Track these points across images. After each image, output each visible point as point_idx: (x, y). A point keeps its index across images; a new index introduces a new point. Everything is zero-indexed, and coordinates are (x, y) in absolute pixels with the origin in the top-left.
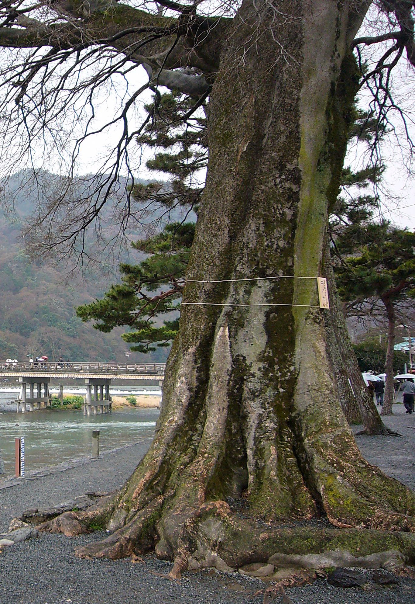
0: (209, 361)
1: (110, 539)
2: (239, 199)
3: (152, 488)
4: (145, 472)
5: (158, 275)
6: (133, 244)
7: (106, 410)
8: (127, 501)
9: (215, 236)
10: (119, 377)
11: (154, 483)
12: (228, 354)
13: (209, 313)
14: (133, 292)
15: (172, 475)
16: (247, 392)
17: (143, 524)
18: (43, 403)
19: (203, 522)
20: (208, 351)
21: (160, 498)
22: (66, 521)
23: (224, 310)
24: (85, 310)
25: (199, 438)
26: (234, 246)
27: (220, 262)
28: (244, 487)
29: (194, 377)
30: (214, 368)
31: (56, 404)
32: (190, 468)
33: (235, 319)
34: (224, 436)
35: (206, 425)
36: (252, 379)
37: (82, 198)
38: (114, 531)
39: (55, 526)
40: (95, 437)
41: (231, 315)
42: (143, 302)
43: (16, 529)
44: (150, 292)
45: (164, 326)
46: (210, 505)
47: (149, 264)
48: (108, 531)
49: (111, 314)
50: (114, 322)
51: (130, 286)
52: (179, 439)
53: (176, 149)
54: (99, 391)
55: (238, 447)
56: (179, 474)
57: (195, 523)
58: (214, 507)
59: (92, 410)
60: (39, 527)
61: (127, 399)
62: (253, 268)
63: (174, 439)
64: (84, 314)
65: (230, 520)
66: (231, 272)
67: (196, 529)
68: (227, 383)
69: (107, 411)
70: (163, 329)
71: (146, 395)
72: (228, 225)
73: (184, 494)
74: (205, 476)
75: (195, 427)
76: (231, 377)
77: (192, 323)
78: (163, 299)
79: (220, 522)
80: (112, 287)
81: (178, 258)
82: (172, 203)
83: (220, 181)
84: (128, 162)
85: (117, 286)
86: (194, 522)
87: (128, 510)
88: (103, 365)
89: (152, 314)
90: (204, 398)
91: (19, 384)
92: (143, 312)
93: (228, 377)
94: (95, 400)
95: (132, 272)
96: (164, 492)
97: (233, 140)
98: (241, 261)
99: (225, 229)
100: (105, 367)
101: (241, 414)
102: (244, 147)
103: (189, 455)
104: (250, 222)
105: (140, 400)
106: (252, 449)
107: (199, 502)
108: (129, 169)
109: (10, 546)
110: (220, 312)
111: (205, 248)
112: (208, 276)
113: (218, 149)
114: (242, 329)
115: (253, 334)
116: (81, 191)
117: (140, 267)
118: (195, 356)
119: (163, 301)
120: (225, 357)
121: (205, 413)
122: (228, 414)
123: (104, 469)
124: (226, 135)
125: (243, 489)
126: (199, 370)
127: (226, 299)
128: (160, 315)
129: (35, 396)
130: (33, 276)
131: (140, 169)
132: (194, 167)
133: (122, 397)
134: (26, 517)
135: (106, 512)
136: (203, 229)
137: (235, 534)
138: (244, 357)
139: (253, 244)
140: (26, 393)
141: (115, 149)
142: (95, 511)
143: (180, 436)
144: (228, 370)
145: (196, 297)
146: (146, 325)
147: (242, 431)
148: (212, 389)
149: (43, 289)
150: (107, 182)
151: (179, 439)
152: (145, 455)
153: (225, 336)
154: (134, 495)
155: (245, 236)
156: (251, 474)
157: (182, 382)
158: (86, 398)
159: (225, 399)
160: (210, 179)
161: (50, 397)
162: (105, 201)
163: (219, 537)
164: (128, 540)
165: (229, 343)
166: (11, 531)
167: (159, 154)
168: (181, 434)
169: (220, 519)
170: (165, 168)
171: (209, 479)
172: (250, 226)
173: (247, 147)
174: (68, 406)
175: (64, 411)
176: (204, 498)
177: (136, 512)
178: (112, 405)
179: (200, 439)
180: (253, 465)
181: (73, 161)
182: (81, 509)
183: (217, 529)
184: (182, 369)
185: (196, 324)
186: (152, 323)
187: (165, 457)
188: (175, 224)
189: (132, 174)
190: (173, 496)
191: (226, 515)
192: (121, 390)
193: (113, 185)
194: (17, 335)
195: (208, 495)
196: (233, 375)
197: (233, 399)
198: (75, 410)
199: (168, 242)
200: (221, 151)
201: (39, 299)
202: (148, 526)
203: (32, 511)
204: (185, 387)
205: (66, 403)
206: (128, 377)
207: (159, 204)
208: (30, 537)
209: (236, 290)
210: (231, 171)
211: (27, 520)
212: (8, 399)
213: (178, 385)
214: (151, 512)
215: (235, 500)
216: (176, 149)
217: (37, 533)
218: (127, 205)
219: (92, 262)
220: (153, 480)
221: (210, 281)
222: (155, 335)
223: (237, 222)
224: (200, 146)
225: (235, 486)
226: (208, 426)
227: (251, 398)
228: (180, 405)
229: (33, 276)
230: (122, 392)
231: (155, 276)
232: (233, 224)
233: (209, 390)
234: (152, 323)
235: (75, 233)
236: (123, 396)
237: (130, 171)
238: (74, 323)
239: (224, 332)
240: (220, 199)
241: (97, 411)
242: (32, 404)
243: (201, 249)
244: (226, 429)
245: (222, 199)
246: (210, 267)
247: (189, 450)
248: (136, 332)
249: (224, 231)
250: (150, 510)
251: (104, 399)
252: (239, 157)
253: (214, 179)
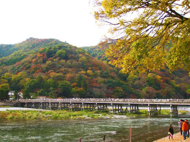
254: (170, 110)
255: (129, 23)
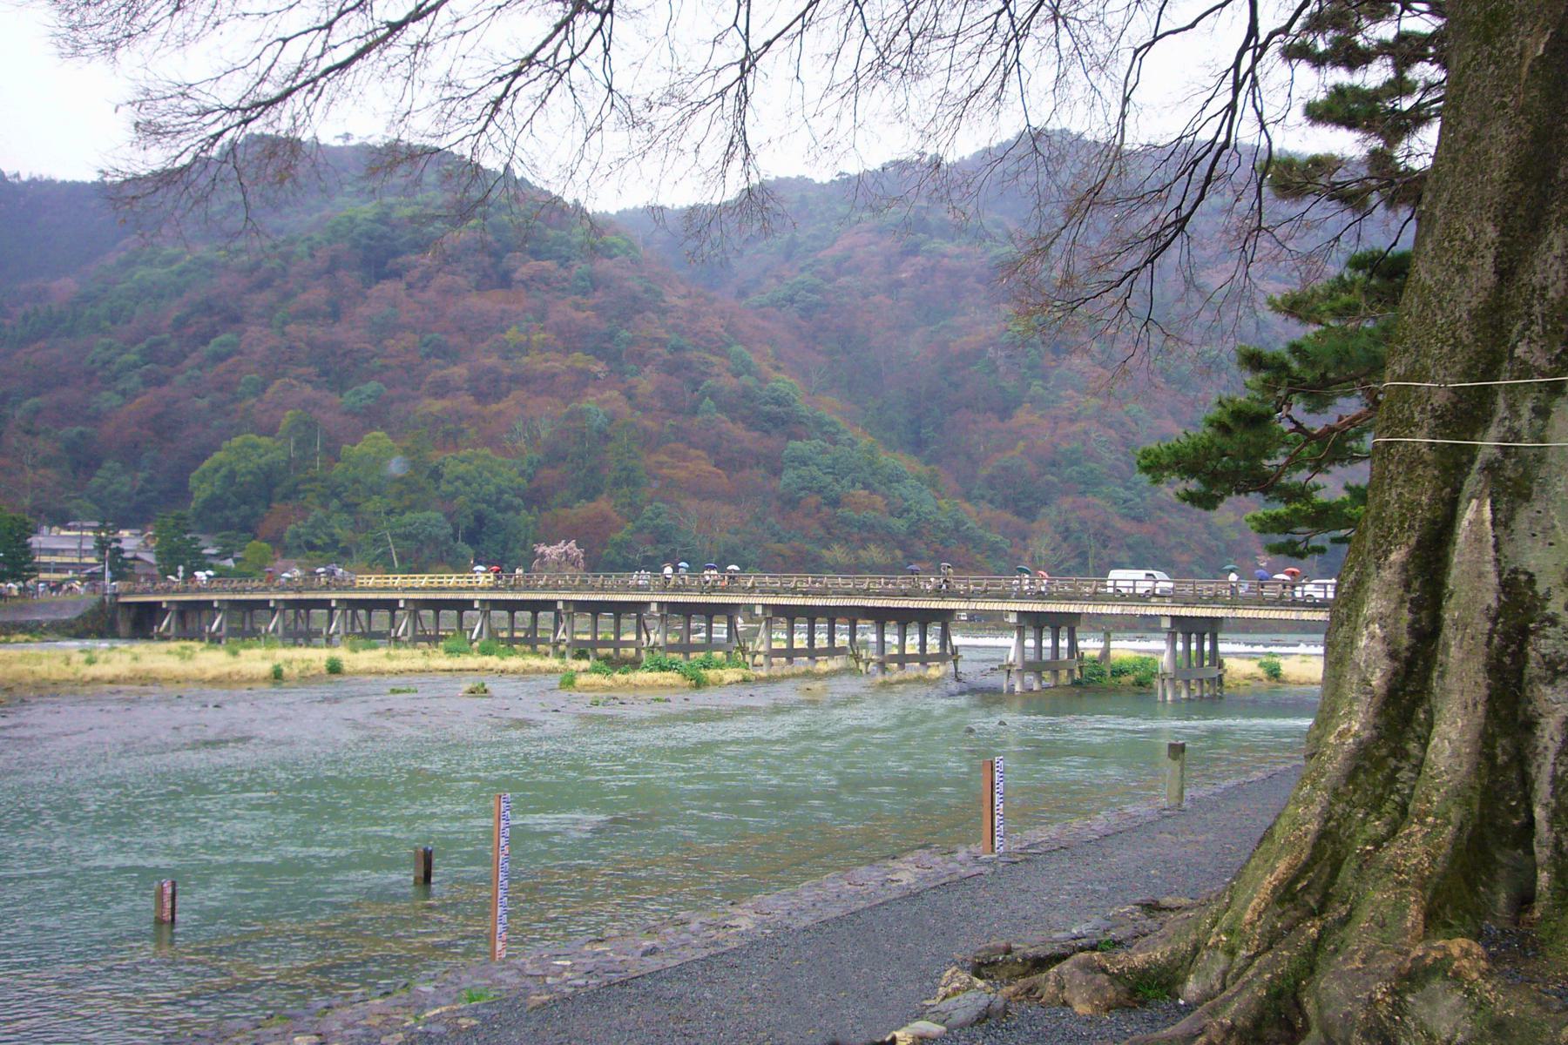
0: (1442, 585)
1: (1183, 1025)
2: (1522, 177)
3: (1293, 898)
4: (1278, 858)
5: (1332, 375)
6: (1271, 302)
7: (1208, 691)
8: (1230, 932)
9: (1461, 270)
10: (1241, 613)
11: (1299, 886)
12: (1489, 568)
13: (1442, 464)
14: (1269, 416)
15: (1344, 867)
16: (1538, 663)
17: (1268, 989)
18: (1064, 673)
19: (1418, 993)
20: (1438, 560)
21: (1313, 926)
22: (1079, 977)
23: (1480, 456)
24: (1157, 456)
25: (1413, 775)
26: (1508, 296)
27: (1471, 336)
28: (1525, 899)
29: (1404, 625)
30: (1453, 601)
31: (1094, 675)
32: (1390, 852)
33: (1509, 479)
34: (1476, 770)
35: (1433, 743)
36: (1550, 631)
37: (1147, 188)
38: (1199, 1003)
39: (1050, 988)
40: (1175, 759)
41: (1499, 468)
42: (1296, 438)
43: (955, 994)
44: (1313, 415)
45: (1346, 495)
46: (1434, 948)
47: (1309, 348)
48: (1181, 1002)
49: (1219, 466)
50: (1227, 486)
51: (1263, 402)
52: (1362, 776)
53: (1376, 75)
54: (1194, 646)
55: (1512, 800)
56: (1360, 866)
57: (1397, 993)
58: (1446, 956)
59: (1176, 691)
60: (1012, 989)
61: (1261, 665)
62: (1558, 351)
63: (1351, 776)
64: (1154, 467)
65: (1487, 989)
66: (1502, 361)
67: (1398, 1008)
68: (1485, 638)
69: (1211, 692)
70: (1343, 504)
71: (1304, 655)
72: (1493, 243)
73: (1372, 918)
74: (1427, 873)
75: (1403, 749)
76: (1496, 624)
77: (1399, 490)
78: (1344, 433)
79: (1461, 993)
80: (1220, 402)
81: (1377, 332)
82: (1364, 202)
83: (1476, 131)
84: (1258, 101)
85: (1232, 401)
86: (1393, 992)
87: (1232, 952)
88: (1205, 586)
89: (1317, 468)
90: (1426, 678)
91: (1011, 628)
92: (1295, 463)
93: (1488, 625)
94: (1184, 666)
95: (1266, 368)
96: (1322, 908)
97: (1509, 26)
98: (1527, 333)
99: (1486, 252)
100: (1210, 589)
101: (1521, 718)
102: (1537, 45)
103: (1387, 818)
104: (1551, 236)
105: (1289, 668)
106: (1546, 805)
107: (1408, 939)
108: (1261, 120)
109: (935, 1040)
110: (1472, 461)
111: (1434, 301)
112: (1442, 373)
113: (1471, 52)
114: (1525, 504)
115: (1552, 518)
116: (1143, 175)
117: (1287, 356)
118: (1407, 571)
119: (1344, 437)
120: (1481, 575)
121: (1430, 713)
122: (1487, 717)
123: (1191, 837)
124: (1494, 17)
125: (1523, 904)
126: (1416, 606)
127: (1486, 429)
128: (1336, 469)
129: (1047, 656)
130: (1045, 378)
131: (1290, 120)
132: (1418, 118)
133: (1250, 659)
134: (981, 964)
135: (1179, 956)
136: (1431, 254)
137: (1499, 1027)
138: (1531, 576)
139: (1557, 292)
140: (1024, 647)
141: (1228, 71)
142: (1155, 952)
143: (1366, 771)
144: (1489, 608)
145: (1409, 424)
146: (1303, 493)
147: (1522, 760)
148: (1447, 655)
149: (1069, 408)
150: (1209, 150)
151: (1362, 776)
152: (1278, 816)
153: (1483, 522)
154: (1248, 916)
155: (1538, 269)
156: (1543, 869)
157: (1372, 637)
158: (1165, 660)
159: (1479, 680)
160: (1451, 126)
161: (1081, 658)
162: (1202, 197)
163: (1457, 1030)
164: (1230, 1031)
165: (1492, 540)
166: (943, 1000)
167: (1335, 87)
168: (1367, 764)
169: (1461, 986)
170: (1350, 119)
171: (1435, 880)
172: (1551, 244)
173: (1546, 44)
174: (1123, 679)
175: (1115, 691)
176: (1421, 927)
177: (1253, 958)
178: (1226, 678)
179: (1416, 779)
180: (1547, 846)
181: (1126, 100)
182: (1120, 943)
183: (1454, 1011)
184: (1373, 604)
185: (1410, 492)
186: (1317, 488)
187: (1327, 821)
188: (1372, 253)
189: (1270, 133)
190: (1345, 921)
191: (1475, 975)
192: (1247, 644)
193: (1223, 158)
194: (1008, 516)
195: (1434, 920)
196: (1501, 620)
197: (1501, 679)
198: (1137, 689)
199: (1356, 297)
200: (1479, 56)
201: (1058, 431)
202: (1279, 995)
203: (995, 950)
204: (1379, 647)
205: (1119, 672)
206: (1262, 614)
207: (1333, 204)
208: (987, 1017)
209: (1513, 409)
210: (1504, 106)
211: (983, 971)
212: (983, 661)
213: (1362, 643)
214: (1289, 958)
215: (1503, 932)
216: (1376, 75)
217: (1005, 1006)
218: (1256, 206)
219: (1171, 343)
220: (1296, 880)
221: (1446, 383)
222: (1325, 517)
223: (1518, 234)
224: (1436, 66)
225: (1502, 898)
226: (1435, 746)
227: (1545, 678)
228: (1366, 693)
229: (1045, 378)
230: (1248, 649)
231: (1323, 376)
232: (1508, 239)
233: (1439, 657)
234: (1317, 488)
235: (1131, 272)
236: (1250, 656)
237: (1263, 127)
238: (1139, 487)
239: (1479, 511)
240: (1475, 177)
241: (1190, 691)
242: (1039, 674)
243: (1426, 304)
244: (1481, 753)
245: (1480, 177)
246: (1446, 349)
247: (1388, 807)
248: (1281, 509)
249: (1483, 257)
250: (1285, 954)
251: (1206, 663)
252: (1525, 69)
253: (1460, 128)
254: (1161, 652)
255: (486, 111)
